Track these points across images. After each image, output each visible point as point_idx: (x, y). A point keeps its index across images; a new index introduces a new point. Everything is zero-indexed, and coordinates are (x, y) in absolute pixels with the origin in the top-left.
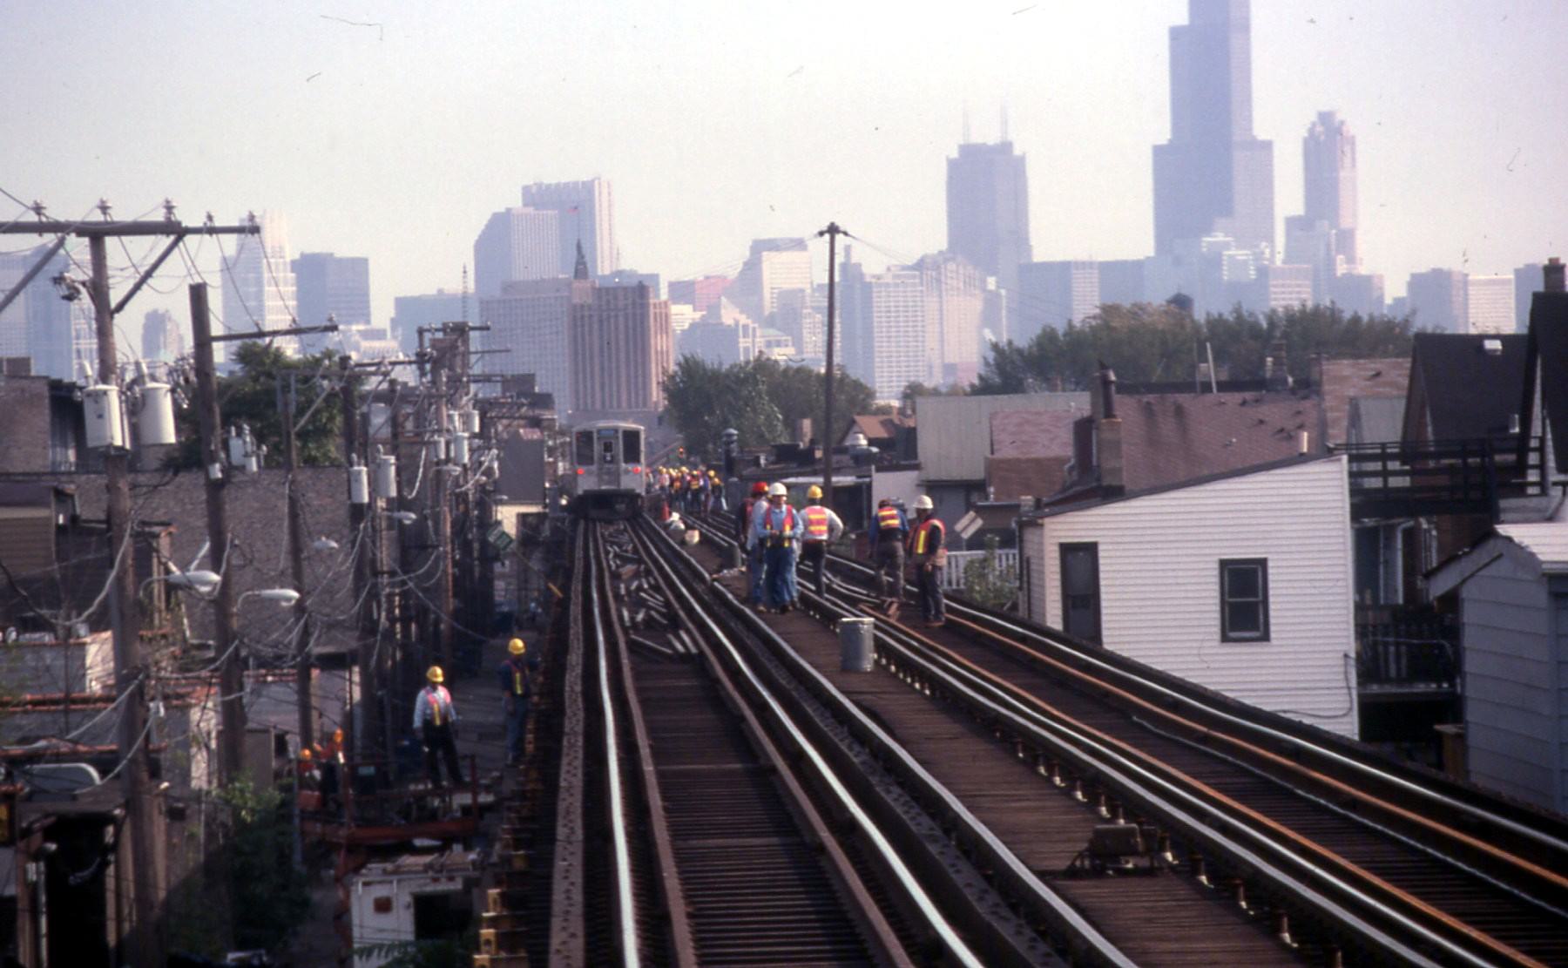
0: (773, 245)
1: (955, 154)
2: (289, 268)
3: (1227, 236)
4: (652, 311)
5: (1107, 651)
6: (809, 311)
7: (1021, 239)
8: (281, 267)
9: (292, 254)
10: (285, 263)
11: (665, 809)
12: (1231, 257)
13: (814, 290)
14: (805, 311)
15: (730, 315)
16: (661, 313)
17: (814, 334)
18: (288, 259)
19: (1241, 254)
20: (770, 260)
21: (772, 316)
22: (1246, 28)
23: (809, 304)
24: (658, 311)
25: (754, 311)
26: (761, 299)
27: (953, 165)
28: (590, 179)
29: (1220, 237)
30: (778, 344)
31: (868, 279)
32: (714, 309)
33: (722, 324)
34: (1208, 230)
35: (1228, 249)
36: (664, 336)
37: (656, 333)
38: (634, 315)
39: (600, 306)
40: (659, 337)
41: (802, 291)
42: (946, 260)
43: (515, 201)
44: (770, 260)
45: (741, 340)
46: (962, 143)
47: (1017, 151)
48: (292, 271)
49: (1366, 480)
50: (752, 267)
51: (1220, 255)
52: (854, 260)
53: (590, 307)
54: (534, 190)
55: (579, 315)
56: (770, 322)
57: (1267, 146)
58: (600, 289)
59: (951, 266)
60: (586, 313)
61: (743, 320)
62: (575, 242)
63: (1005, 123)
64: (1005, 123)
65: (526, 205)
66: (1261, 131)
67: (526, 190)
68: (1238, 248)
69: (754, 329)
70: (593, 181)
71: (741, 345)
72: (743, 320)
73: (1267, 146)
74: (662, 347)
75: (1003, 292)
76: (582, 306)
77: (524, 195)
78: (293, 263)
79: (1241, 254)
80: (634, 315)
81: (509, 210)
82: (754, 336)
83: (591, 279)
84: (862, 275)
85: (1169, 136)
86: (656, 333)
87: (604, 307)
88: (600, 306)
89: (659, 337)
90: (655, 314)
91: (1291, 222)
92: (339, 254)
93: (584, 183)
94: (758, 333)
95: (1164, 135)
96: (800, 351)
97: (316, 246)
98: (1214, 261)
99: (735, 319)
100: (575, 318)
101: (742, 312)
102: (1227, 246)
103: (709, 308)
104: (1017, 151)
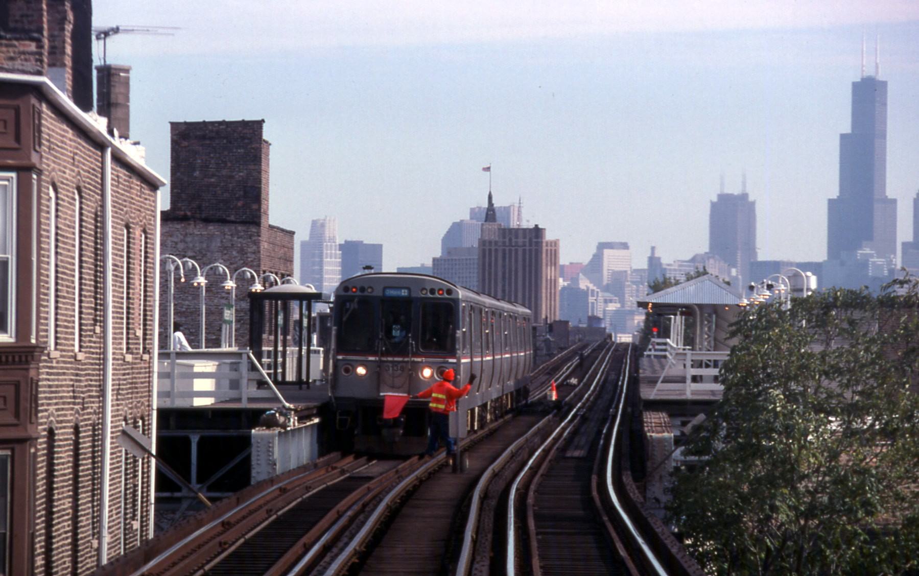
0: (610, 246)
1: (715, 199)
2: (338, 247)
3: (871, 250)
4: (544, 249)
5: (662, 411)
6: (629, 283)
7: (750, 247)
8: (334, 248)
9: (340, 240)
10: (336, 246)
11: (538, 547)
12: (874, 263)
13: (632, 272)
14: (627, 283)
15: (584, 284)
16: (551, 250)
17: (632, 296)
18: (337, 243)
19: (880, 261)
20: (607, 252)
21: (608, 285)
22: (884, 136)
23: (629, 279)
24: (549, 248)
25: (598, 282)
26: (602, 276)
27: (714, 206)
28: (507, 205)
29: (868, 251)
30: (611, 301)
31: (664, 266)
32: (575, 280)
33: (579, 288)
34: (860, 247)
35: (872, 258)
36: (553, 268)
37: (547, 265)
38: (530, 251)
39: (504, 243)
40: (549, 268)
41: (626, 272)
42: (709, 258)
43: (466, 217)
44: (607, 252)
45: (590, 298)
46: (719, 193)
47: (751, 198)
48: (340, 250)
49: (279, 323)
50: (597, 259)
51: (868, 260)
52: (657, 255)
53: (496, 243)
54: (477, 210)
55: (487, 248)
56: (607, 289)
57: (894, 201)
58: (504, 230)
59: (711, 261)
60: (493, 248)
61: (591, 286)
62: (488, 193)
63: (744, 184)
64: (744, 184)
65: (471, 218)
66: (890, 193)
67: (472, 210)
68: (878, 258)
69: (598, 292)
70: (509, 207)
71: (590, 301)
72: (591, 286)
73: (894, 201)
74: (551, 277)
75: (740, 277)
76: (490, 242)
77: (471, 213)
78: (340, 245)
79: (880, 261)
80: (530, 251)
81: (462, 221)
82: (597, 296)
83: (498, 222)
84: (661, 264)
85: (838, 194)
86: (547, 265)
87: (507, 244)
88: (504, 243)
89: (549, 268)
90: (547, 250)
91: (905, 245)
92: (365, 242)
93: (505, 207)
94: (600, 294)
95: (835, 193)
96: (623, 306)
97: (354, 237)
98: (864, 265)
99: (587, 286)
100: (484, 251)
101: (591, 283)
102: (871, 256)
103: (572, 279)
104: (751, 199)
